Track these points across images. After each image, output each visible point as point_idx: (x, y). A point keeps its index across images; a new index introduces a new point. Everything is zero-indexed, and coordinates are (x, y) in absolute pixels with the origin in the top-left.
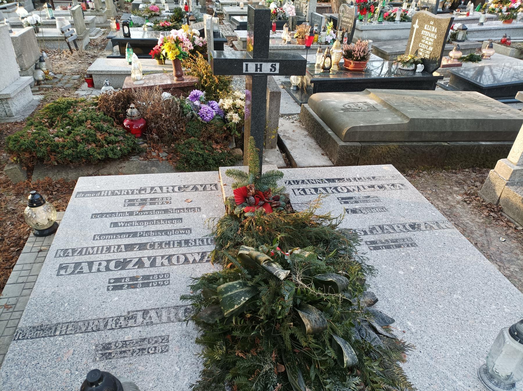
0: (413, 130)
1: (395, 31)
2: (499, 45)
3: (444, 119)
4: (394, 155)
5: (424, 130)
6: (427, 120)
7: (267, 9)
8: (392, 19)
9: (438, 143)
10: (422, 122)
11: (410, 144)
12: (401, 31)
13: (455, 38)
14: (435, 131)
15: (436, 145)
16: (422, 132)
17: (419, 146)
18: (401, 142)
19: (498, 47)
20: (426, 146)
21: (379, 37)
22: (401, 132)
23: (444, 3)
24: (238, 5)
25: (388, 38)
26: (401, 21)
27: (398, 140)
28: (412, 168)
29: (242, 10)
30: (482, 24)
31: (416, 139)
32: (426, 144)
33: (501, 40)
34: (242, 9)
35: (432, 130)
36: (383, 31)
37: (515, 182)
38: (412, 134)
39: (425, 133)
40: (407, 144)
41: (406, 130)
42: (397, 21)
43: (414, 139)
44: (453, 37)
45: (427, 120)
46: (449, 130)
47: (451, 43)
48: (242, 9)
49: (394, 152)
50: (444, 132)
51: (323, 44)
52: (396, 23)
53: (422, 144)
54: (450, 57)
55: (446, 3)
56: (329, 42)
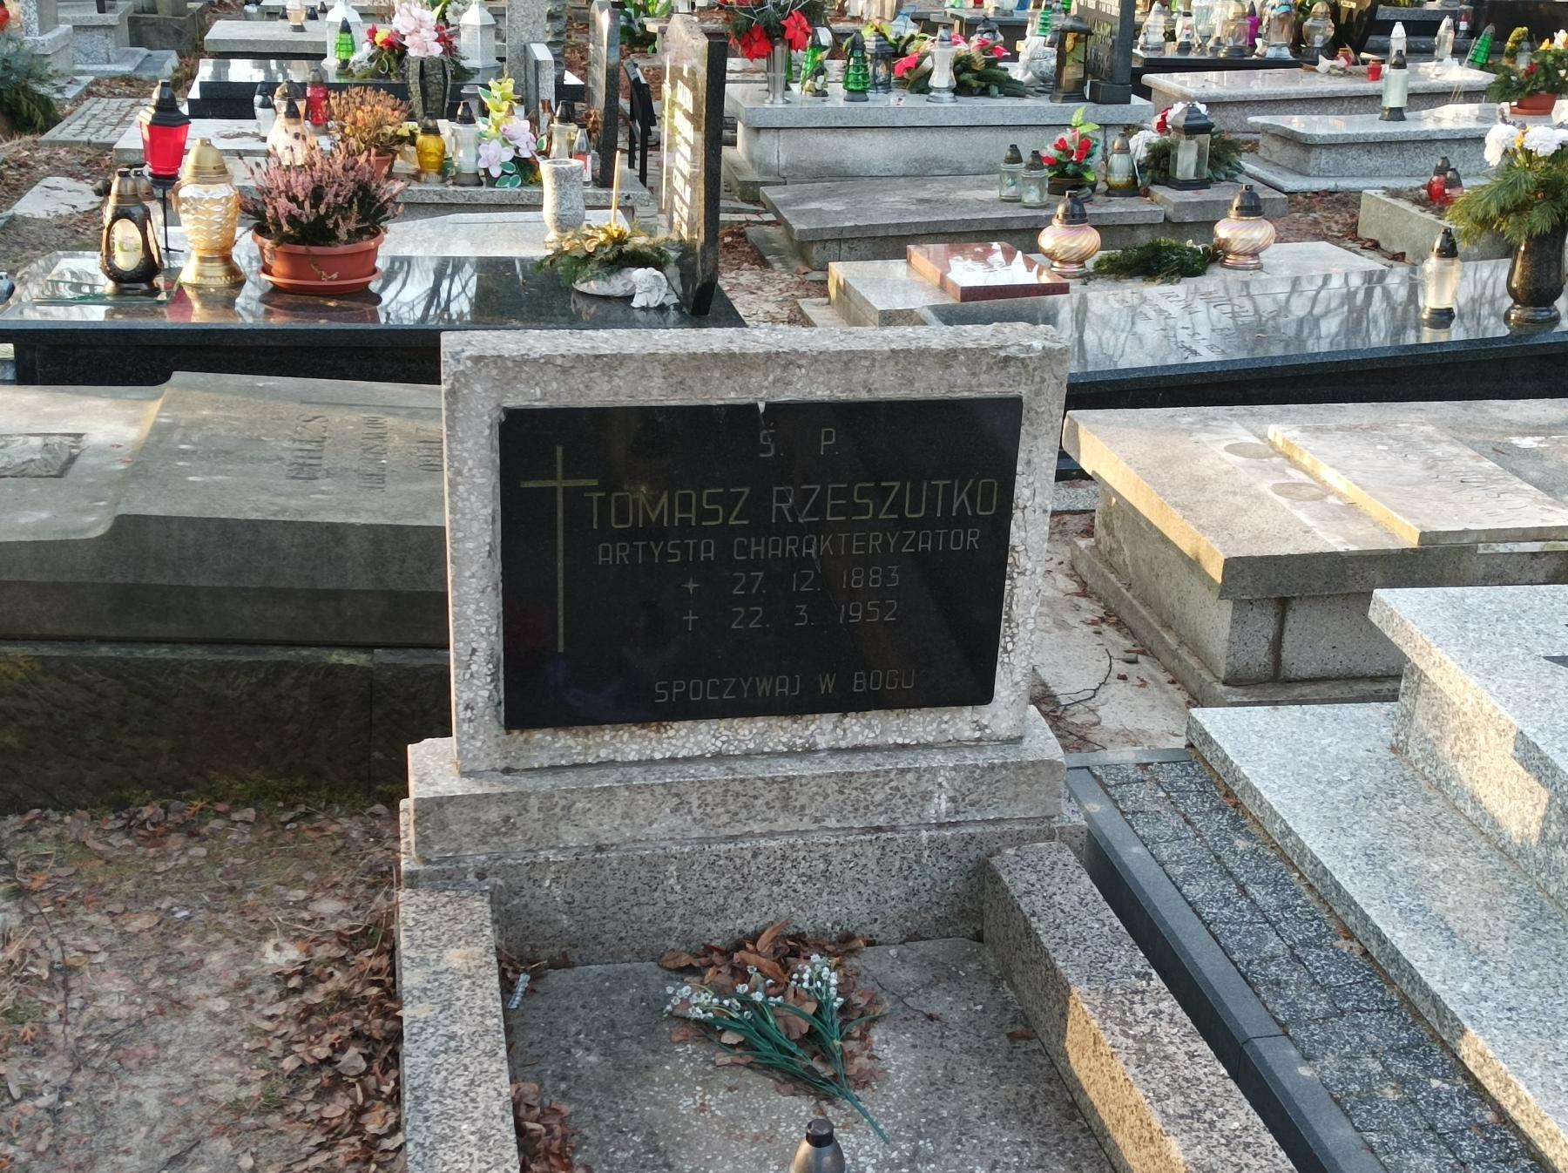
0: (130, 579)
1: (928, 136)
2: (1415, 210)
3: (332, 528)
4: (29, 713)
5: (204, 581)
6: (228, 530)
7: (1117, 28)
8: (919, 83)
9: (305, 652)
10: (192, 534)
11: (121, 652)
12: (959, 137)
13: (1166, 171)
14: (274, 583)
15: (280, 668)
16: (193, 592)
17: (174, 668)
18: (80, 640)
19: (1411, 217)
20: (222, 669)
21: (848, 163)
22: (57, 586)
23: (1301, 24)
24: (285, 17)
25: (900, 167)
26: (960, 90)
27: (51, 628)
28: (170, 787)
29: (299, 37)
30: (1397, 114)
31: (171, 629)
32: (231, 655)
33: (1429, 187)
34: (300, 29)
35: (255, 581)
36: (867, 134)
37: (464, 872)
38: (127, 598)
39: (216, 594)
40: (104, 651)
41: (85, 578)
42: (939, 90)
43: (154, 629)
44: (1157, 167)
45: (227, 528)
46: (363, 583)
47: (1147, 193)
48: (300, 29)
49: (24, 695)
50: (335, 595)
51: (464, 180)
52: (939, 100)
53: (198, 653)
54: (1046, 254)
55: (1309, 22)
56: (495, 172)
